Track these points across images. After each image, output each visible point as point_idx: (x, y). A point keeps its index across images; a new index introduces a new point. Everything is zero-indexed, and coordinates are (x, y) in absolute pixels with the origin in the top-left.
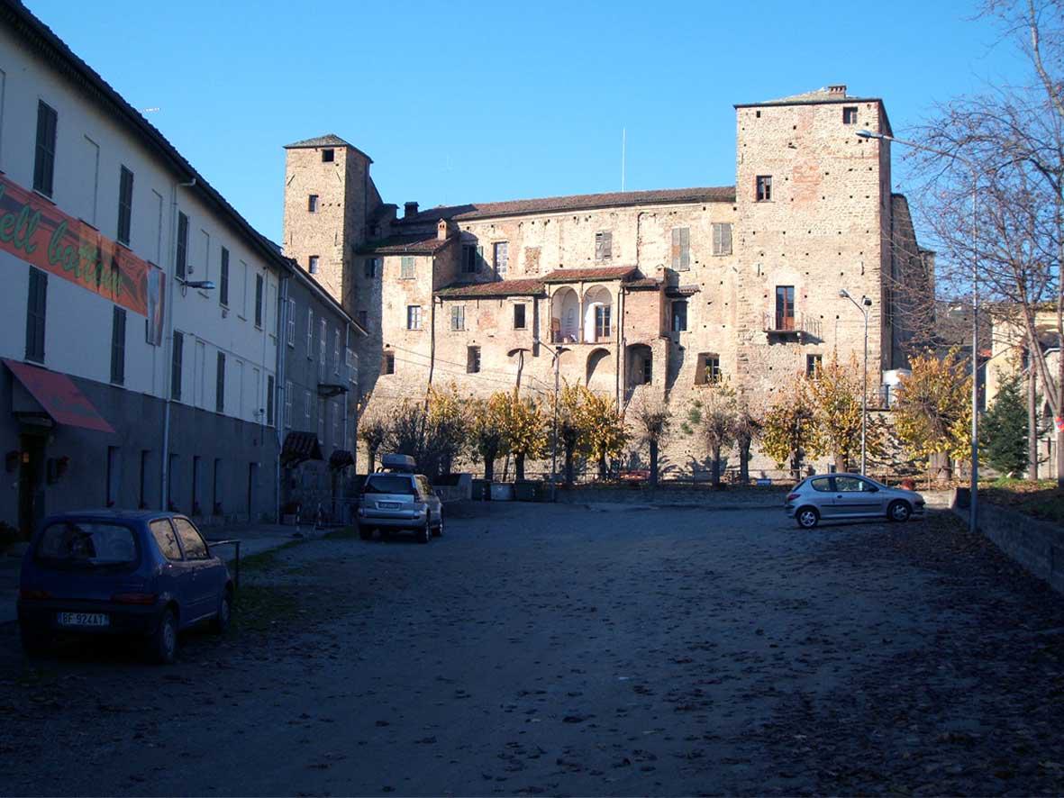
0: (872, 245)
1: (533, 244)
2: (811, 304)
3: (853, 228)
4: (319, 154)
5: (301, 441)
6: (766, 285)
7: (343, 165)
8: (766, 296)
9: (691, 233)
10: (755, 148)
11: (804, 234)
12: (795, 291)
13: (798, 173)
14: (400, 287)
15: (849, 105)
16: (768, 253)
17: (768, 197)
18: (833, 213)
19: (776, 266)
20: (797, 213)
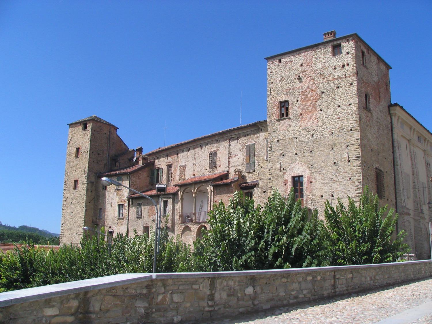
0: (354, 139)
1: (182, 164)
2: (314, 188)
3: (341, 129)
4: (81, 127)
5: (421, 189)
6: (286, 176)
7: (90, 131)
8: (285, 185)
9: (255, 146)
10: (278, 84)
11: (309, 138)
12: (304, 179)
13: (304, 95)
14: (116, 194)
15: (335, 43)
16: (286, 154)
17: (287, 115)
18: (327, 120)
19: (292, 163)
20: (304, 123)
